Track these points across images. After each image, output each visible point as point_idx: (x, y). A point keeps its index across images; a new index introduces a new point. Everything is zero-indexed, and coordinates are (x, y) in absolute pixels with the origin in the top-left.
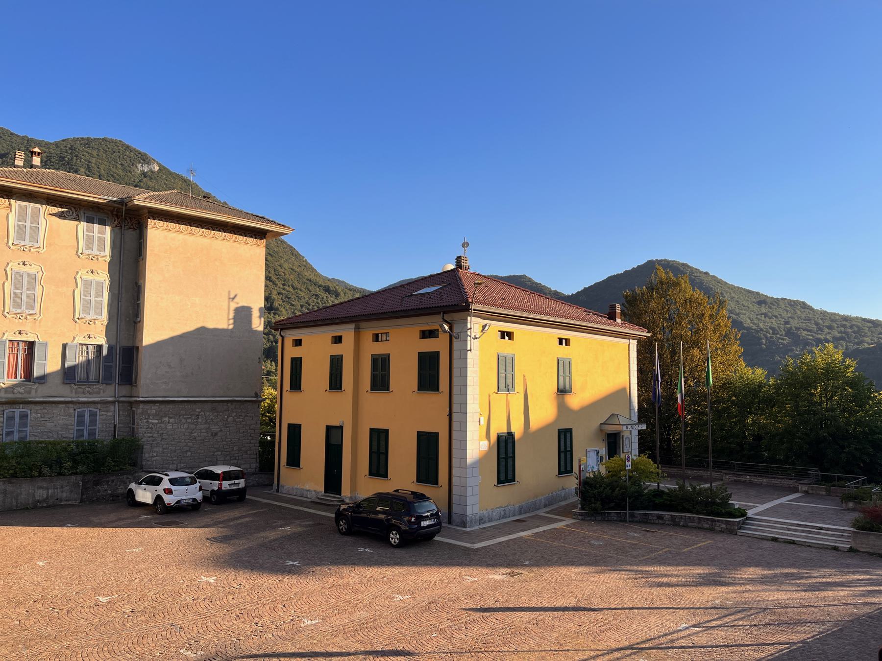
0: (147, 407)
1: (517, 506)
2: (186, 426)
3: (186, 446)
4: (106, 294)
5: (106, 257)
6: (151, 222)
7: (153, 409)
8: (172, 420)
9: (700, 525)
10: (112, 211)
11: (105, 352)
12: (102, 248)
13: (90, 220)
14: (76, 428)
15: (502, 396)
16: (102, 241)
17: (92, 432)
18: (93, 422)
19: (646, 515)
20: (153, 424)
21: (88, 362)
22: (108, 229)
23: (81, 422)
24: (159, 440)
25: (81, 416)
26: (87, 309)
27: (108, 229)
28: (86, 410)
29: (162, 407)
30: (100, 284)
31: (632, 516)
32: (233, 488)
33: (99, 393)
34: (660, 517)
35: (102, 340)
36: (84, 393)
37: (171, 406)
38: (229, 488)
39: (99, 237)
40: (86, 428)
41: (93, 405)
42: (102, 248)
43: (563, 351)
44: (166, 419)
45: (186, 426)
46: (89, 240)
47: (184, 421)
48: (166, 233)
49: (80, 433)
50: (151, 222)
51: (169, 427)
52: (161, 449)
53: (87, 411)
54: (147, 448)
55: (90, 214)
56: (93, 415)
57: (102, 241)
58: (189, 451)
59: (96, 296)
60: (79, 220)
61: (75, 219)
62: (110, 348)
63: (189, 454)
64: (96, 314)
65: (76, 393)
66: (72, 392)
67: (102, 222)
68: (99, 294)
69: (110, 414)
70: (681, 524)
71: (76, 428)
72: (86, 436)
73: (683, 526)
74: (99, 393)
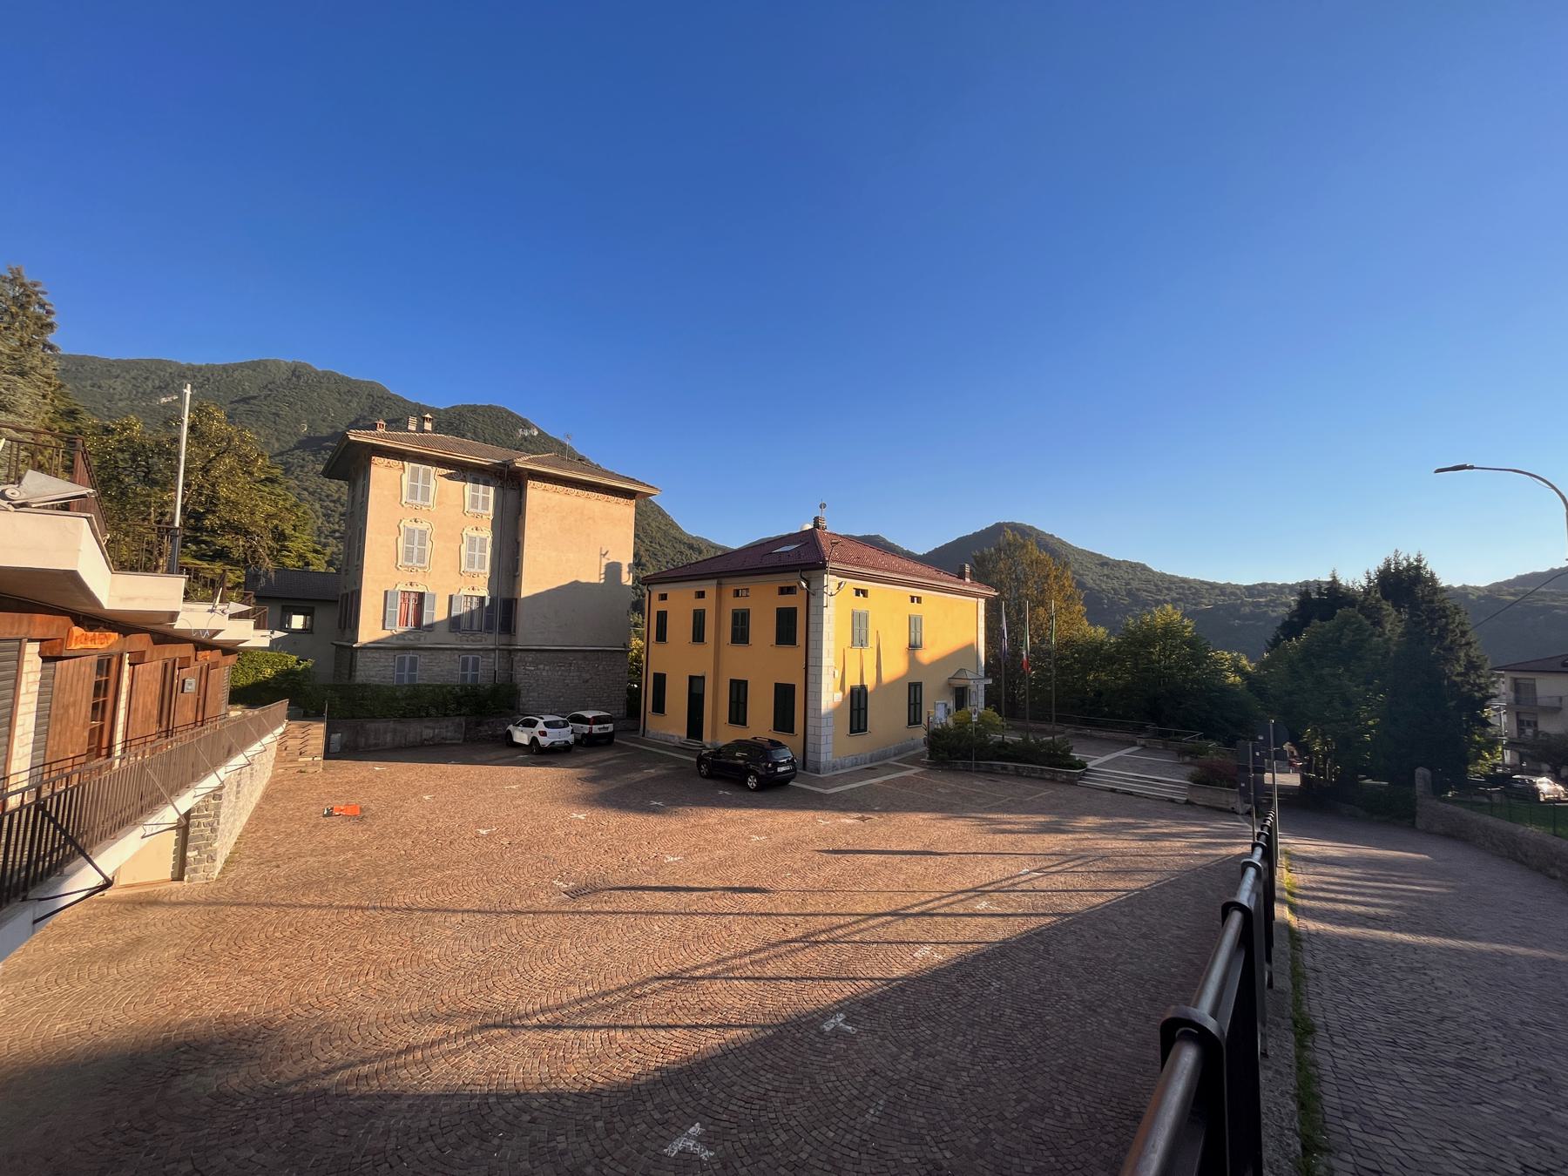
7: (530, 657)
11: (487, 603)
13: (476, 481)
16: (486, 500)
18: (476, 668)
21: (472, 612)
22: (492, 489)
25: (465, 661)
26: (471, 564)
27: (492, 489)
31: (978, 766)
34: (1004, 768)
35: (484, 593)
40: (470, 673)
46: (475, 499)
56: (476, 661)
67: (486, 484)
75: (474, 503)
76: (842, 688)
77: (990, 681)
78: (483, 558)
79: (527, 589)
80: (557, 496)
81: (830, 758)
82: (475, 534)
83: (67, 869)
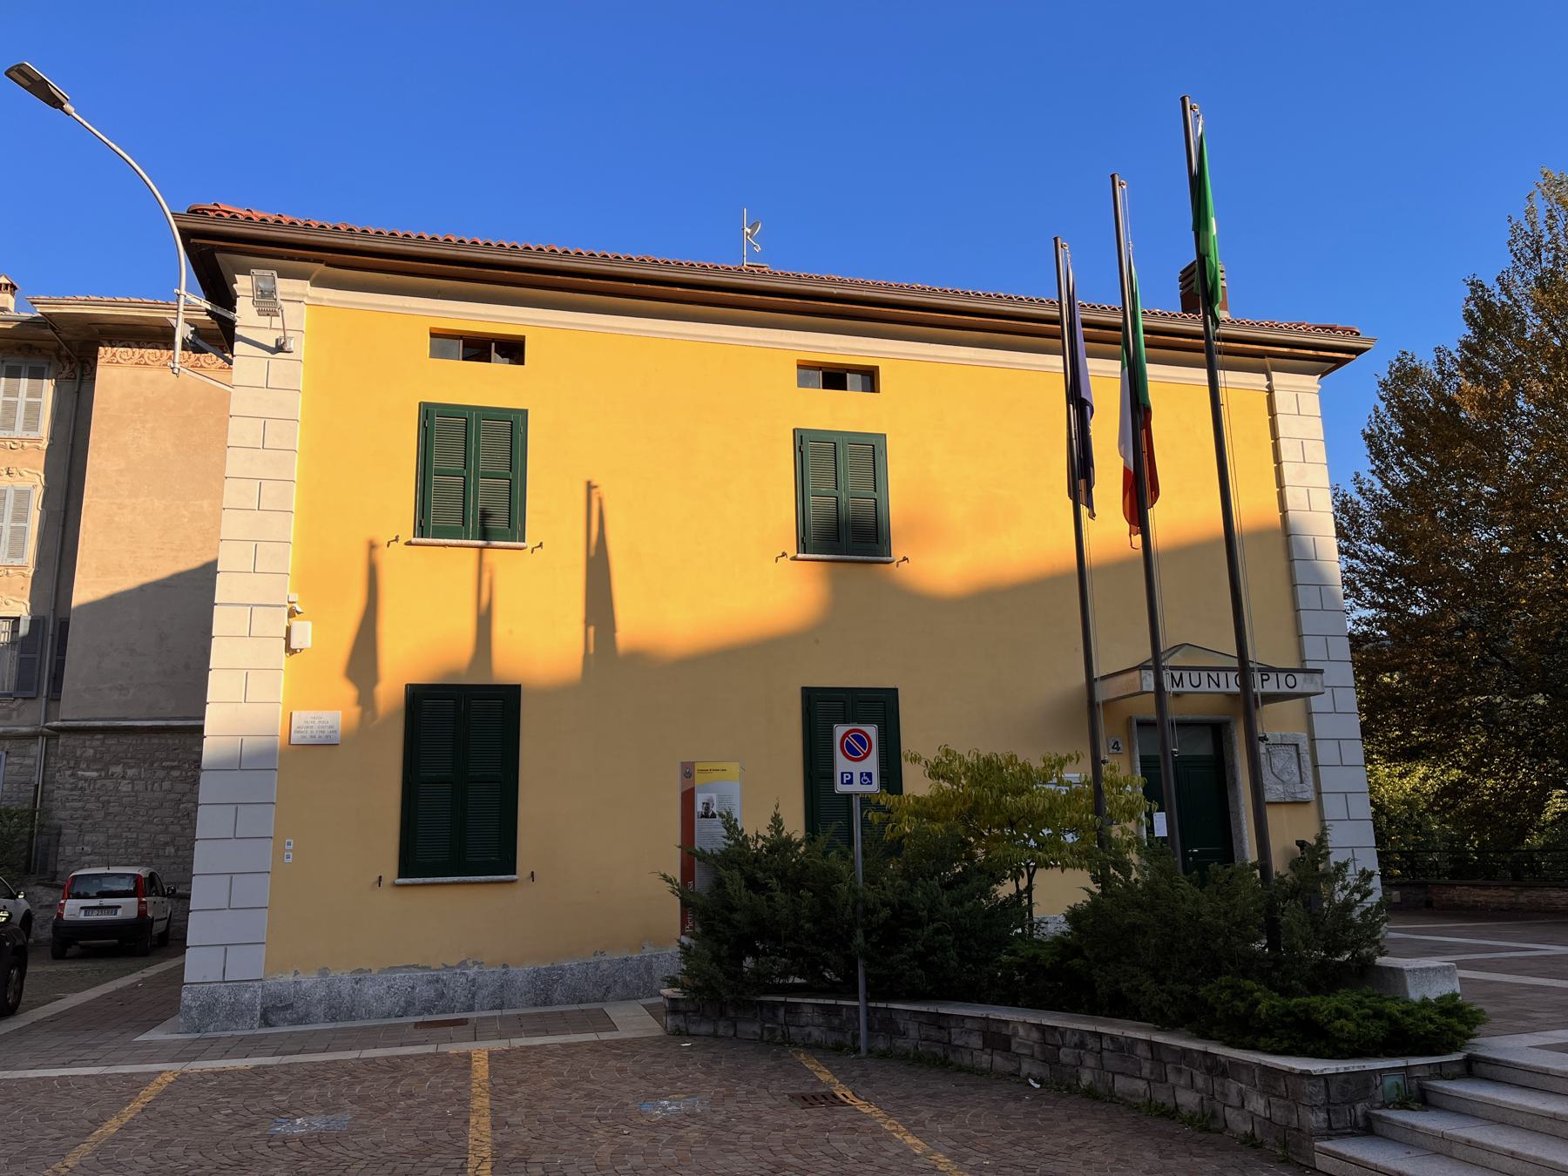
1: (521, 973)
2: (166, 785)
4: (35, 515)
5: (40, 440)
6: (105, 353)
8: (130, 772)
9: (1162, 1096)
10: (58, 350)
11: (24, 629)
12: (31, 424)
15: (455, 561)
16: (32, 410)
19: (938, 1020)
22: (48, 386)
24: (99, 815)
27: (48, 386)
29: (111, 741)
30: (23, 496)
31: (886, 1025)
32: (94, 917)
34: (997, 1039)
38: (82, 917)
42: (31, 424)
44: (118, 769)
47: (161, 774)
48: (138, 371)
50: (105, 353)
51: (125, 787)
52: (102, 838)
54: (69, 833)
57: (32, 410)
58: (172, 842)
59: (15, 519)
62: (34, 623)
63: (170, 850)
67: (36, 374)
68: (20, 515)
70: (1086, 1078)
73: (1091, 1094)
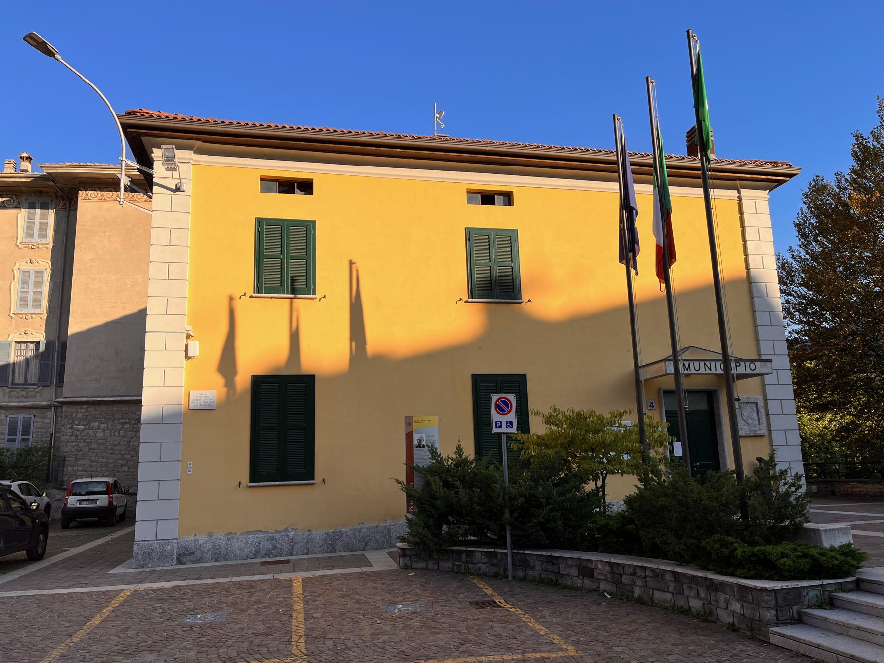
0: (71, 409)
1: (318, 534)
2: (122, 433)
3: (122, 458)
5: (47, 243)
6: (82, 194)
7: (81, 412)
8: (102, 426)
9: (680, 602)
11: (42, 348)
13: (32, 206)
14: (7, 437)
15: (277, 306)
16: (43, 227)
17: (25, 441)
18: (26, 430)
19: (553, 560)
20: (78, 430)
21: (27, 360)
22: (51, 213)
23: (12, 429)
25: (13, 423)
26: (23, 303)
27: (51, 213)
28: (19, 416)
29: (91, 409)
30: (39, 274)
31: (523, 563)
32: (85, 505)
33: (35, 397)
34: (586, 570)
35: (41, 337)
36: (18, 397)
37: (103, 408)
38: (78, 505)
39: (41, 223)
40: (18, 437)
41: (27, 411)
42: (43, 234)
43: (493, 218)
44: (96, 424)
45: (122, 433)
46: (30, 227)
47: (119, 427)
49: (11, 442)
50: (82, 194)
51: (100, 434)
52: (88, 462)
53: (20, 417)
54: (70, 460)
55: (32, 199)
56: (27, 422)
57: (43, 227)
58: (126, 464)
59: (36, 287)
60: (19, 208)
61: (16, 208)
62: (48, 344)
63: (125, 468)
64: (34, 307)
65: (9, 397)
66: (4, 396)
67: (45, 207)
68: (38, 285)
69: (47, 421)
70: (637, 592)
71: (7, 437)
72: (18, 445)
73: (640, 601)
74: (35, 397)
75: (29, 232)
76: (227, 361)
77: (828, 422)
78: (38, 297)
79: (74, 328)
80: (105, 205)
81: (169, 531)
82: (29, 267)
83: (827, 633)
